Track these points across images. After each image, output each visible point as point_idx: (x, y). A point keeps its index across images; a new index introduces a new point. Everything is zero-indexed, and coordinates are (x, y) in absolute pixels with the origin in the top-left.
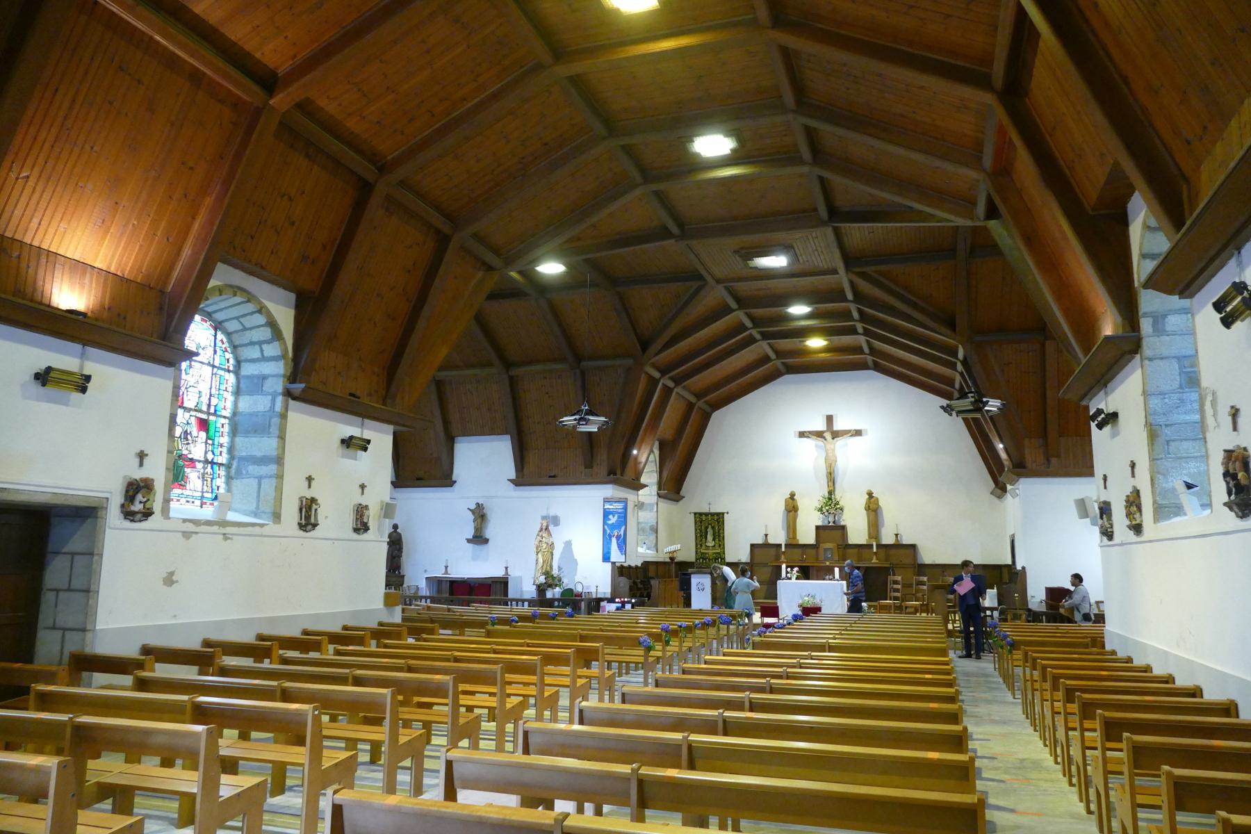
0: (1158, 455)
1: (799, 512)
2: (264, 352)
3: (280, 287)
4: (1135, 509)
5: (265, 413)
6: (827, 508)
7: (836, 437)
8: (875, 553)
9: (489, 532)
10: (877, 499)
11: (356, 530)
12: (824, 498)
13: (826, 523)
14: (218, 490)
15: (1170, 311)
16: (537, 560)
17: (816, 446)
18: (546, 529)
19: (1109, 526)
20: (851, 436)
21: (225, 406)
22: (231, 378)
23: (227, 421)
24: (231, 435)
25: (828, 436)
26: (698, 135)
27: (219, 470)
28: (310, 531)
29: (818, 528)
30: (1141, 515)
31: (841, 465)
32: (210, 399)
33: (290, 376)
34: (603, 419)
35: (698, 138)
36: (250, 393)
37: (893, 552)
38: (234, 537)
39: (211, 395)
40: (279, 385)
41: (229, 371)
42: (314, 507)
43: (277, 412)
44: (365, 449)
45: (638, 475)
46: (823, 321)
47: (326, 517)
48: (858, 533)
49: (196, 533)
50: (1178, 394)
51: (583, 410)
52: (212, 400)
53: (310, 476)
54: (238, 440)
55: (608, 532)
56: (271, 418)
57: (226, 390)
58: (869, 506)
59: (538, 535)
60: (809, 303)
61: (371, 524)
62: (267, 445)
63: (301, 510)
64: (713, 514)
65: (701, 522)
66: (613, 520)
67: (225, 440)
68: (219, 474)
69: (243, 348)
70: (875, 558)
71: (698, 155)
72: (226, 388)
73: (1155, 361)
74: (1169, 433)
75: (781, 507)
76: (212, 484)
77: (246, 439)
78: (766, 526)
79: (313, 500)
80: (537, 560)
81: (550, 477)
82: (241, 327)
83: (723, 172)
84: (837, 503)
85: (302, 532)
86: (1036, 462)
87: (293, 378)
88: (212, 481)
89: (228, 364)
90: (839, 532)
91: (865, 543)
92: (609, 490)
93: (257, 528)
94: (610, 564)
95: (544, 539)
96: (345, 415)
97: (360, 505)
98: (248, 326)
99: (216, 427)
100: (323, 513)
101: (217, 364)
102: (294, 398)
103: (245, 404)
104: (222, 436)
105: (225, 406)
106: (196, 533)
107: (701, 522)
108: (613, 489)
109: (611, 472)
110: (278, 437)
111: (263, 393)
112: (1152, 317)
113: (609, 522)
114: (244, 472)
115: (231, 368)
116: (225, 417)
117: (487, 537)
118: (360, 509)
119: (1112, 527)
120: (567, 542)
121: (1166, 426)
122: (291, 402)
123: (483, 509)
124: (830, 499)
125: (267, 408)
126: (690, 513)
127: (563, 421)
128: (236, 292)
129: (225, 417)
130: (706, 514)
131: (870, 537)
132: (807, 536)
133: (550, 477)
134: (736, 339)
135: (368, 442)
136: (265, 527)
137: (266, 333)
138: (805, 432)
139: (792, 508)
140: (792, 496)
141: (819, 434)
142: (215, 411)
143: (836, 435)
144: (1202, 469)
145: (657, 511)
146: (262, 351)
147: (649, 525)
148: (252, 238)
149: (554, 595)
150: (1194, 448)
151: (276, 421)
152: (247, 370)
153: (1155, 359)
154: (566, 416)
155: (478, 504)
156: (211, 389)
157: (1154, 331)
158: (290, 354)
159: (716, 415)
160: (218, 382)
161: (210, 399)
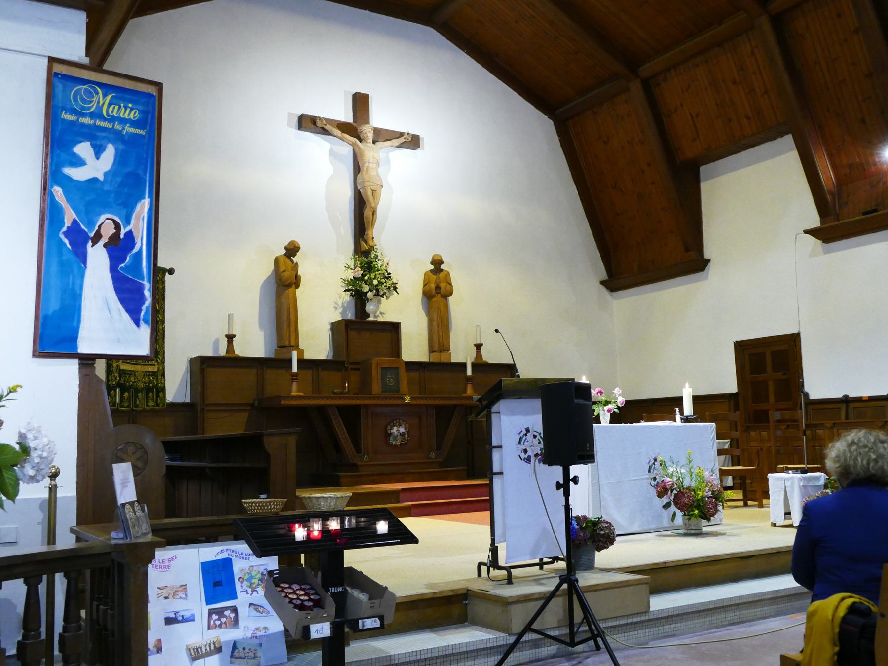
10: (448, 274)
17: (332, 153)
55: (70, 216)
94: (73, 366)
140: (292, 250)
149: (139, 509)
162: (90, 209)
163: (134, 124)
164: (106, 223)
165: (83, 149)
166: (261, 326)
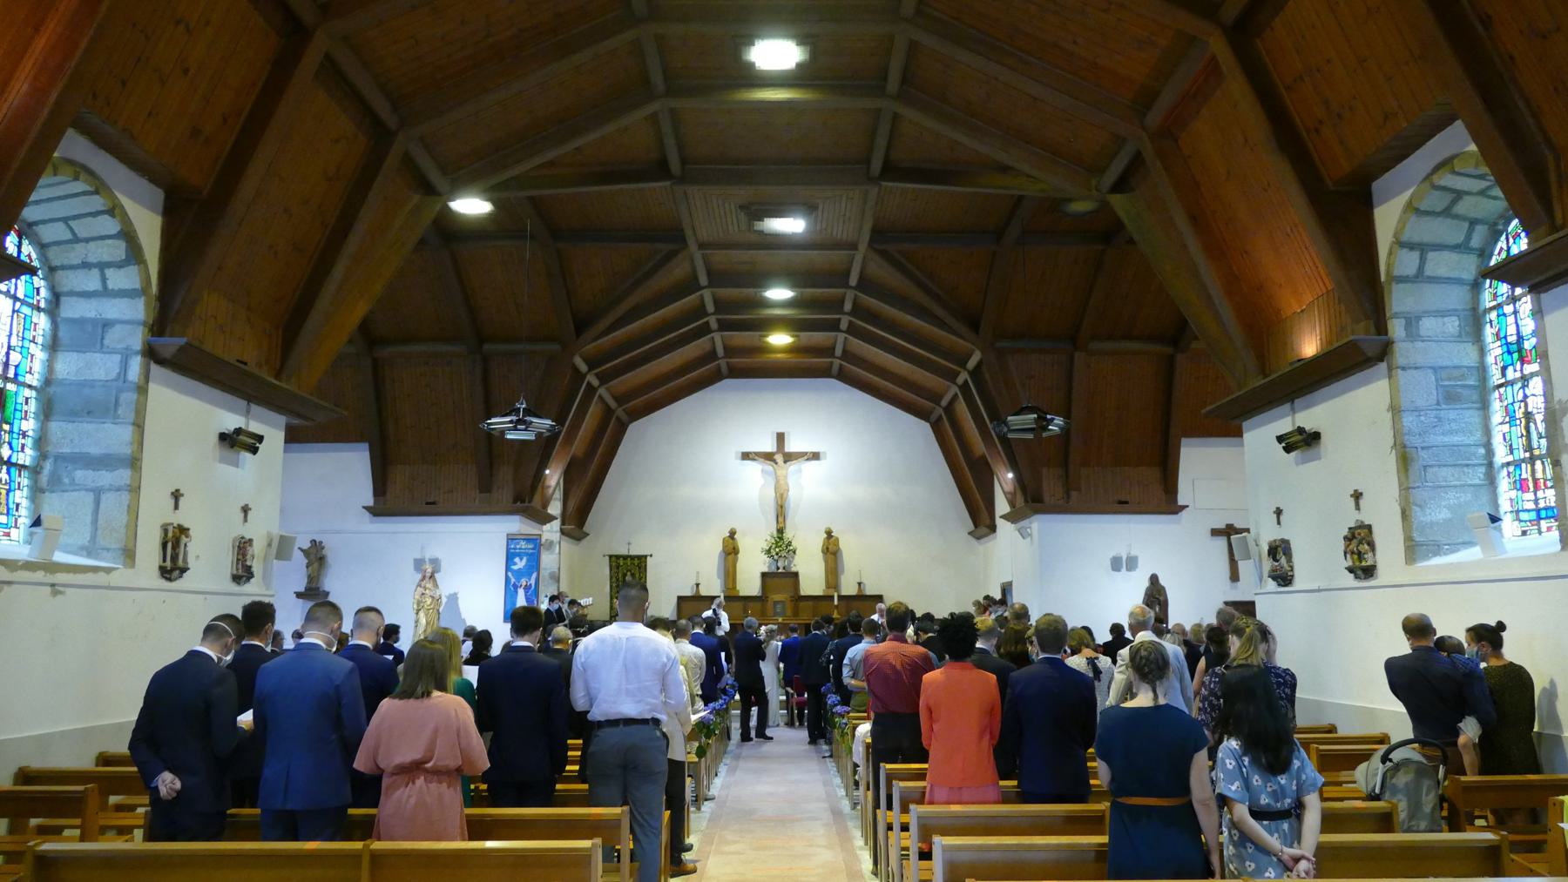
0: (1415, 482)
1: (739, 555)
2: (108, 282)
3: (143, 176)
4: (1366, 547)
5: (109, 383)
6: (777, 550)
7: (789, 461)
8: (837, 607)
9: (857, 585)
10: (837, 539)
11: (237, 579)
12: (772, 537)
13: (773, 569)
14: (17, 510)
15: (1425, 312)
16: (417, 622)
18: (431, 577)
19: (1290, 569)
20: (807, 459)
21: (31, 368)
22: (43, 321)
23: (34, 394)
24: (42, 418)
25: (779, 458)
26: (762, 37)
27: (20, 476)
28: (175, 580)
29: (764, 575)
30: (1374, 555)
31: (793, 495)
32: (8, 354)
33: (153, 325)
34: (549, 422)
35: (760, 41)
36: (79, 348)
37: (856, 604)
38: (69, 591)
39: (9, 347)
40: (136, 339)
41: (39, 309)
42: (184, 539)
43: (131, 382)
44: (254, 450)
45: (545, 505)
46: (801, 312)
47: (198, 557)
48: (812, 581)
49: (9, 583)
50: (1434, 412)
51: (520, 408)
52: (11, 356)
53: (177, 491)
54: (55, 427)
55: (513, 580)
56: (120, 391)
57: (33, 341)
58: (827, 548)
59: (419, 585)
60: (793, 286)
61: (255, 570)
62: (115, 437)
63: (164, 546)
64: (632, 558)
65: (618, 568)
66: (520, 564)
67: (29, 425)
68: (19, 483)
69: (69, 273)
70: (836, 611)
71: (752, 65)
72: (34, 337)
73: (1408, 371)
74: (1426, 456)
75: (718, 547)
76: (7, 500)
77: (70, 426)
78: (698, 573)
79: (183, 530)
80: (417, 622)
81: (427, 503)
82: (69, 236)
83: (776, 94)
84: (790, 544)
85: (163, 580)
86: (1054, 495)
87: (160, 324)
88: (7, 494)
89: (38, 298)
90: (790, 581)
91: (821, 594)
92: (515, 524)
93: (102, 574)
95: (427, 591)
96: (229, 397)
97: (243, 538)
98: (82, 234)
99: (16, 403)
100: (196, 550)
101: (20, 295)
102: (161, 362)
103: (68, 366)
104: (26, 419)
105: (31, 368)
106: (9, 583)
107: (618, 568)
108: (520, 522)
109: (519, 498)
110: (134, 424)
111: (104, 350)
112: (1405, 318)
113: (515, 568)
114: (66, 481)
115: (42, 305)
116: (30, 387)
117: (327, 589)
118: (242, 546)
119: (1292, 570)
120: (450, 595)
121: (1423, 448)
122: (154, 367)
123: (323, 548)
124: (781, 538)
125: (113, 375)
126: (604, 556)
127: (491, 424)
128: (79, 173)
129: (30, 387)
130: (625, 558)
131: (828, 586)
132: (749, 585)
133: (427, 503)
134: (692, 325)
135: (260, 439)
136: (114, 573)
137: (118, 250)
138: (750, 453)
139: (731, 550)
140: (732, 534)
141: (768, 457)
142: (16, 375)
143: (789, 457)
144: (1462, 500)
145: (560, 553)
146: (104, 280)
147: (548, 571)
148: (124, 83)
150: (1453, 476)
151: (129, 397)
152: (72, 309)
153: (1410, 368)
154: (496, 416)
155: (315, 541)
156: (10, 336)
157: (1407, 336)
158: (154, 289)
159: (634, 429)
160: (22, 326)
161: (8, 354)
162: (518, 579)
163: (532, 549)
164: (524, 582)
165: (517, 560)
166: (719, 577)
